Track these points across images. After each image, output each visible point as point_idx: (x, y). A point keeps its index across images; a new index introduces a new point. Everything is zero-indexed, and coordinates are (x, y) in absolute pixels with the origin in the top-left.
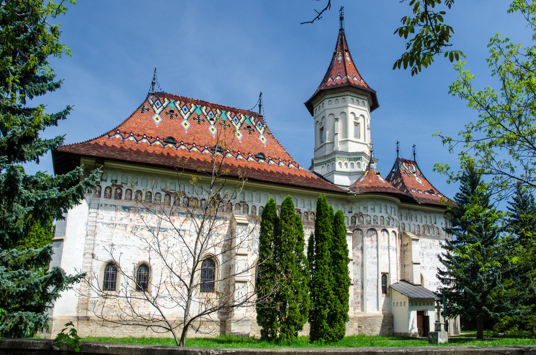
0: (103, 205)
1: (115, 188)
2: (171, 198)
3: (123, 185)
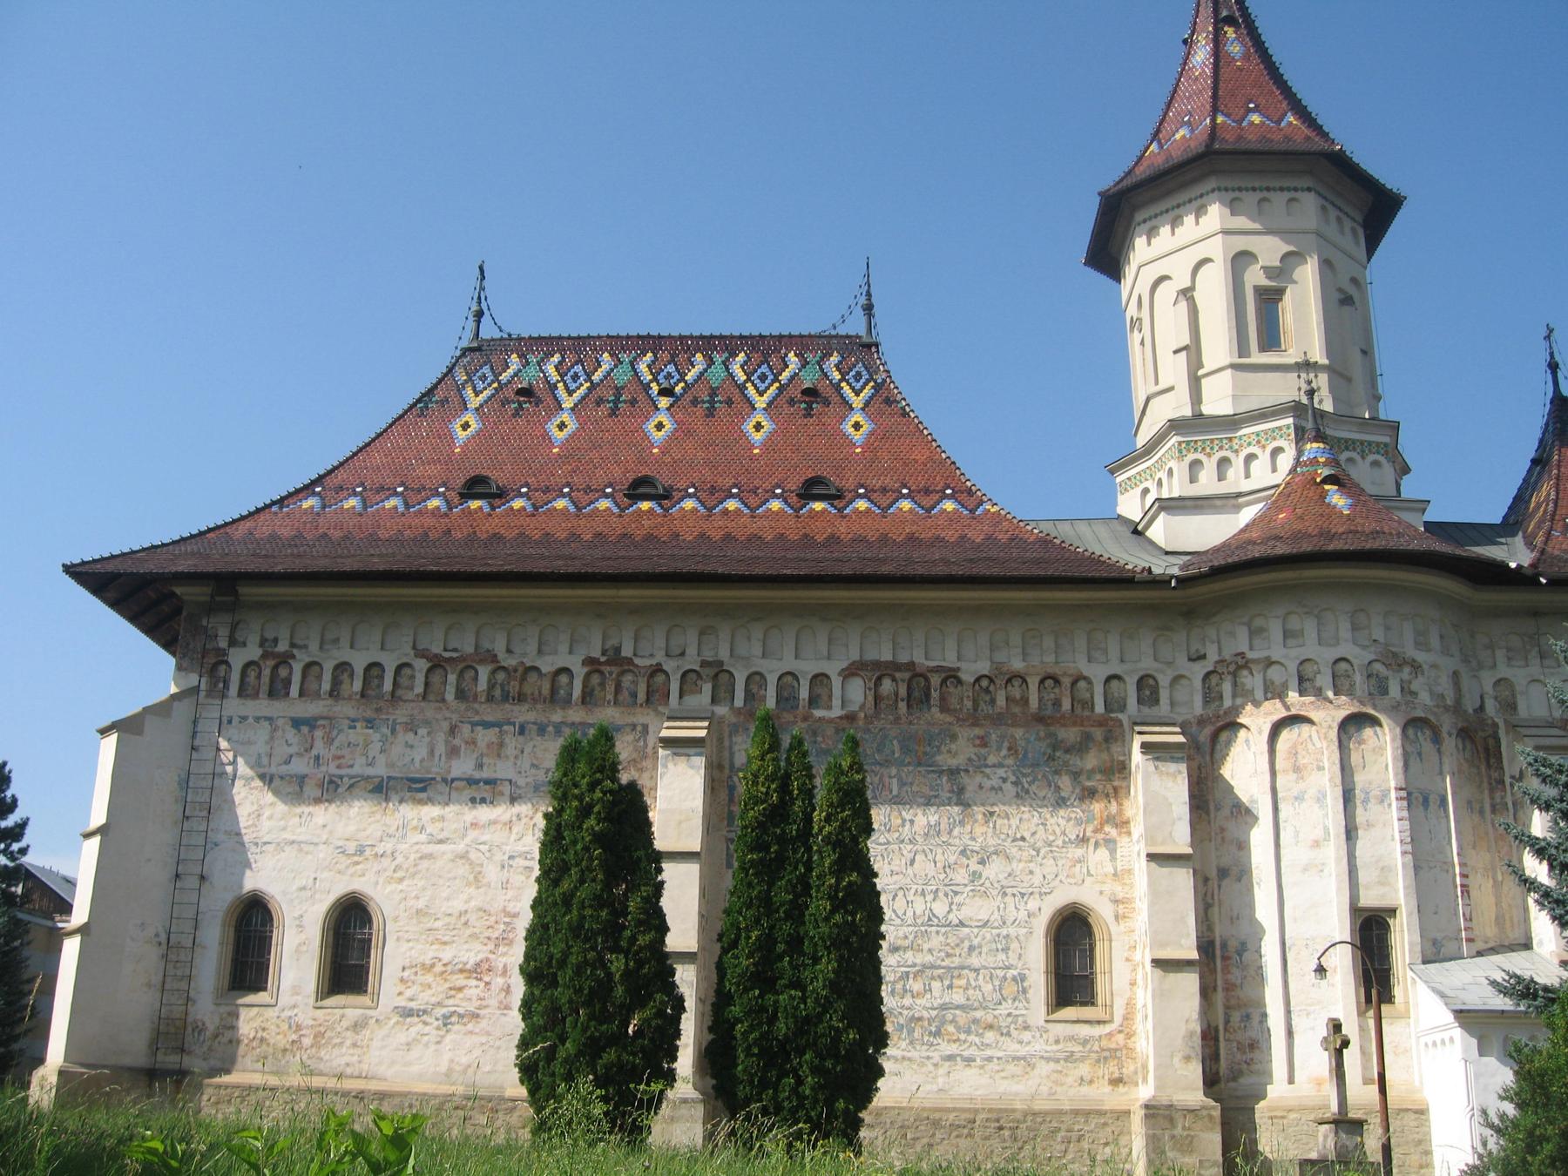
0: (235, 721)
1: (271, 663)
2: (449, 676)
3: (295, 651)
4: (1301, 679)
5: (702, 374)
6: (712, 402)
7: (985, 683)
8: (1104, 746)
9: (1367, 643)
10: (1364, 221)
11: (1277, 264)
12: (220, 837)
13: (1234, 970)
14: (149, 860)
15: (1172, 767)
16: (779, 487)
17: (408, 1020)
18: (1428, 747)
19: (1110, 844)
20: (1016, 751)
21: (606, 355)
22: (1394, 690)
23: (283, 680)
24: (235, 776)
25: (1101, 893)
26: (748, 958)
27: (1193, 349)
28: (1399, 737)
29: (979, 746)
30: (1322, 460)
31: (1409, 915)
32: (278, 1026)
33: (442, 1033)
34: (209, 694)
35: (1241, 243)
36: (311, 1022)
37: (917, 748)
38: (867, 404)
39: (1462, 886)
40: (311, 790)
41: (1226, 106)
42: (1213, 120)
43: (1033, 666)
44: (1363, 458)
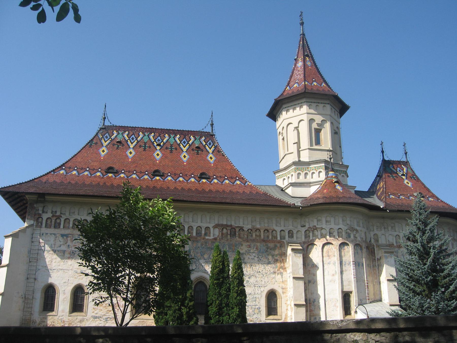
0: (44, 234)
1: (55, 218)
3: (62, 215)
4: (330, 233)
5: (168, 140)
6: (171, 149)
7: (250, 231)
8: (280, 248)
9: (346, 224)
10: (340, 111)
11: (320, 123)
12: (40, 267)
13: (312, 307)
14: (20, 274)
15: (299, 255)
16: (193, 174)
17: (96, 319)
18: (359, 251)
19: (281, 274)
20: (258, 249)
21: (141, 133)
22: (352, 236)
23: (58, 223)
24: (44, 250)
25: (279, 286)
26: (216, 308)
27: (298, 143)
28: (353, 249)
29: (249, 247)
30: (334, 176)
31: (355, 293)
32: (58, 321)
33: (105, 323)
34: (36, 226)
35: (312, 116)
36: (68, 320)
37: (232, 247)
38: (213, 152)
39: (367, 286)
40: (67, 255)
41: (307, 79)
42: (305, 83)
43: (262, 227)
44: (340, 174)
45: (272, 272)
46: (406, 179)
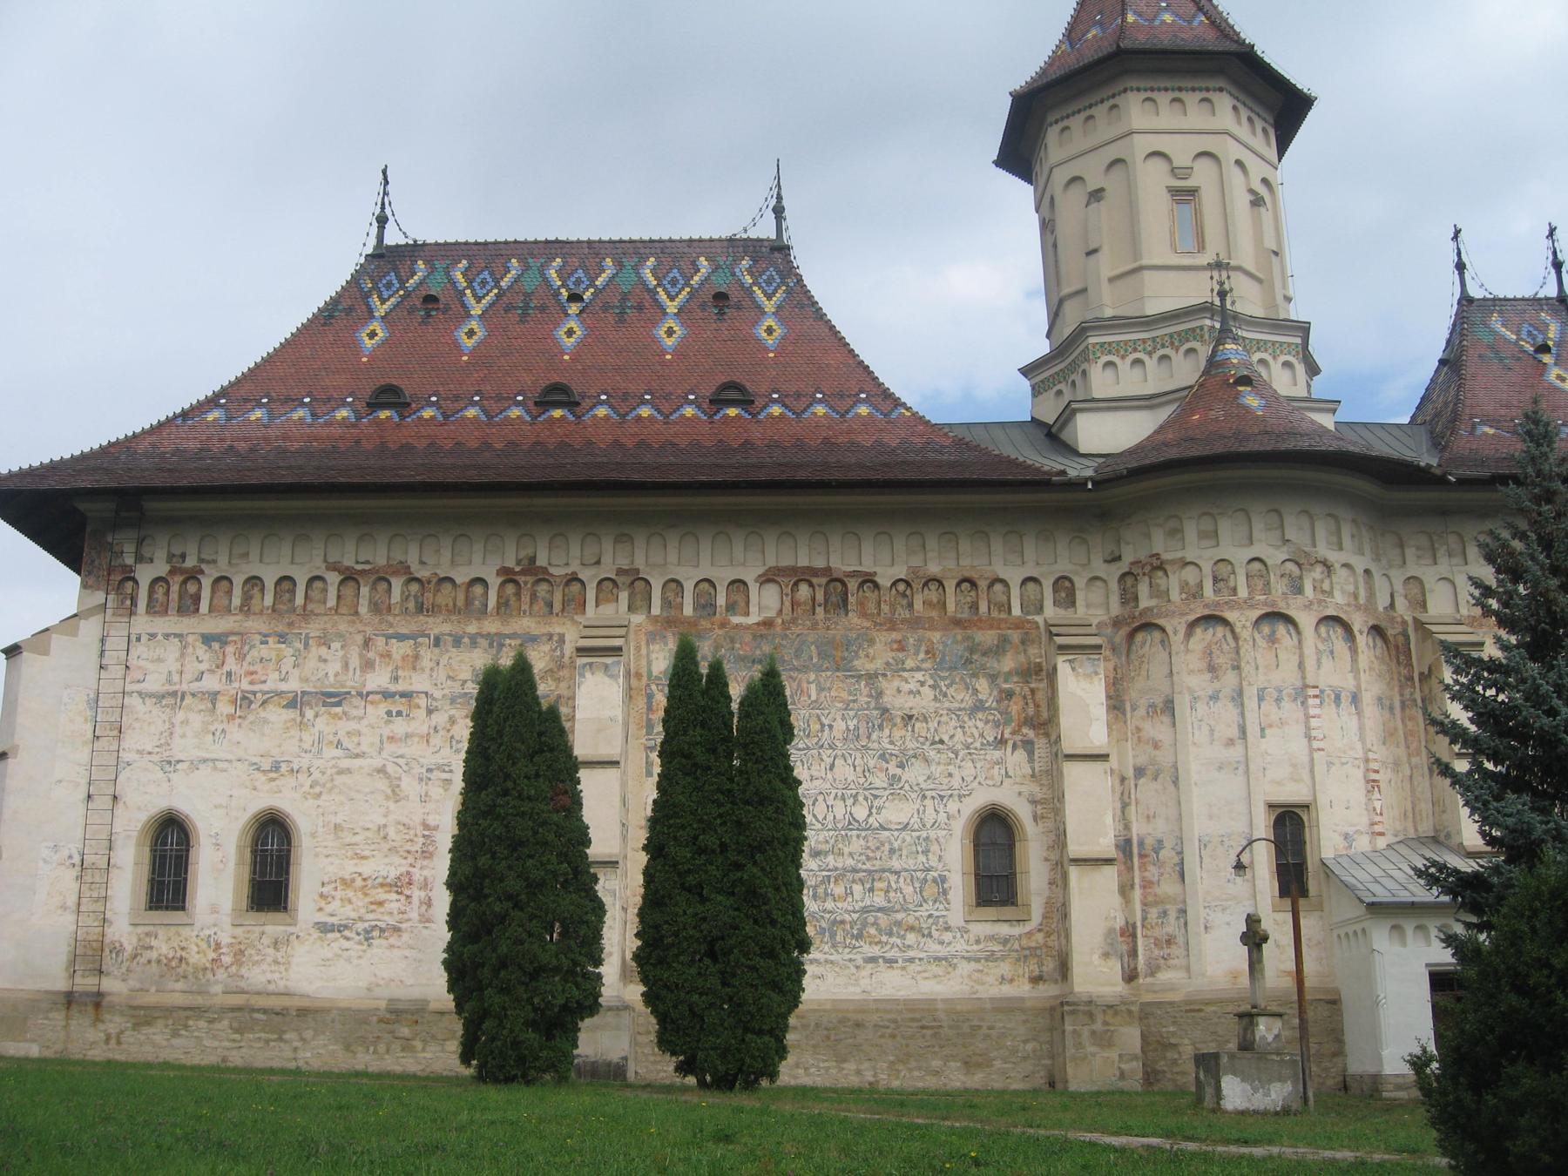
0: (144, 638)
1: (179, 578)
3: (203, 566)
8: (1021, 648)
10: (1276, 121)
17: (330, 935)
29: (898, 650)
38: (779, 308)
44: (1274, 358)
45: (991, 739)
46: (1556, 364)
